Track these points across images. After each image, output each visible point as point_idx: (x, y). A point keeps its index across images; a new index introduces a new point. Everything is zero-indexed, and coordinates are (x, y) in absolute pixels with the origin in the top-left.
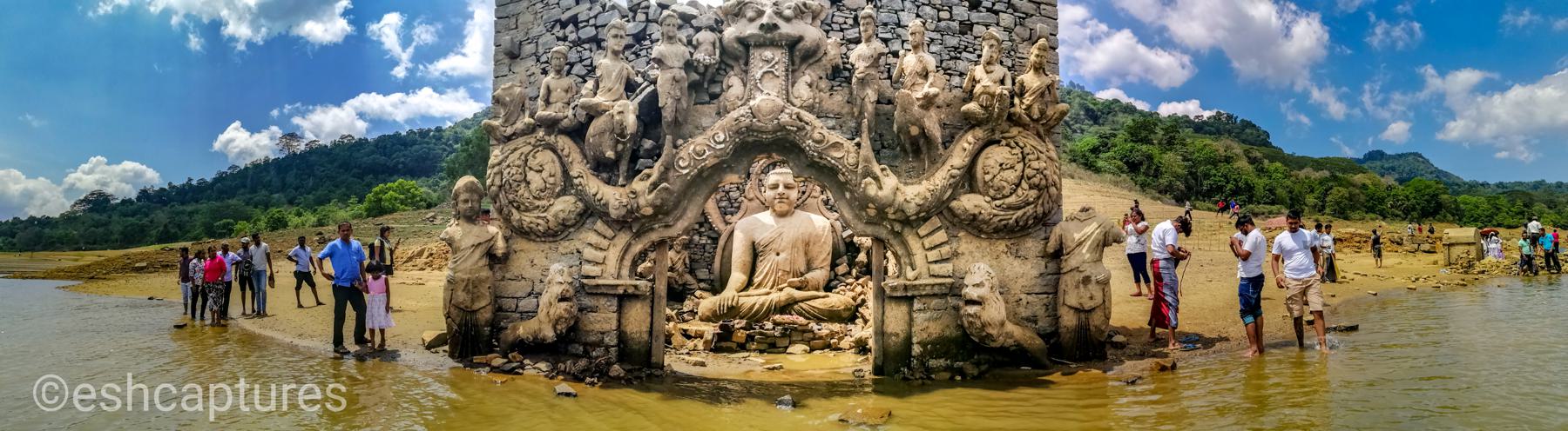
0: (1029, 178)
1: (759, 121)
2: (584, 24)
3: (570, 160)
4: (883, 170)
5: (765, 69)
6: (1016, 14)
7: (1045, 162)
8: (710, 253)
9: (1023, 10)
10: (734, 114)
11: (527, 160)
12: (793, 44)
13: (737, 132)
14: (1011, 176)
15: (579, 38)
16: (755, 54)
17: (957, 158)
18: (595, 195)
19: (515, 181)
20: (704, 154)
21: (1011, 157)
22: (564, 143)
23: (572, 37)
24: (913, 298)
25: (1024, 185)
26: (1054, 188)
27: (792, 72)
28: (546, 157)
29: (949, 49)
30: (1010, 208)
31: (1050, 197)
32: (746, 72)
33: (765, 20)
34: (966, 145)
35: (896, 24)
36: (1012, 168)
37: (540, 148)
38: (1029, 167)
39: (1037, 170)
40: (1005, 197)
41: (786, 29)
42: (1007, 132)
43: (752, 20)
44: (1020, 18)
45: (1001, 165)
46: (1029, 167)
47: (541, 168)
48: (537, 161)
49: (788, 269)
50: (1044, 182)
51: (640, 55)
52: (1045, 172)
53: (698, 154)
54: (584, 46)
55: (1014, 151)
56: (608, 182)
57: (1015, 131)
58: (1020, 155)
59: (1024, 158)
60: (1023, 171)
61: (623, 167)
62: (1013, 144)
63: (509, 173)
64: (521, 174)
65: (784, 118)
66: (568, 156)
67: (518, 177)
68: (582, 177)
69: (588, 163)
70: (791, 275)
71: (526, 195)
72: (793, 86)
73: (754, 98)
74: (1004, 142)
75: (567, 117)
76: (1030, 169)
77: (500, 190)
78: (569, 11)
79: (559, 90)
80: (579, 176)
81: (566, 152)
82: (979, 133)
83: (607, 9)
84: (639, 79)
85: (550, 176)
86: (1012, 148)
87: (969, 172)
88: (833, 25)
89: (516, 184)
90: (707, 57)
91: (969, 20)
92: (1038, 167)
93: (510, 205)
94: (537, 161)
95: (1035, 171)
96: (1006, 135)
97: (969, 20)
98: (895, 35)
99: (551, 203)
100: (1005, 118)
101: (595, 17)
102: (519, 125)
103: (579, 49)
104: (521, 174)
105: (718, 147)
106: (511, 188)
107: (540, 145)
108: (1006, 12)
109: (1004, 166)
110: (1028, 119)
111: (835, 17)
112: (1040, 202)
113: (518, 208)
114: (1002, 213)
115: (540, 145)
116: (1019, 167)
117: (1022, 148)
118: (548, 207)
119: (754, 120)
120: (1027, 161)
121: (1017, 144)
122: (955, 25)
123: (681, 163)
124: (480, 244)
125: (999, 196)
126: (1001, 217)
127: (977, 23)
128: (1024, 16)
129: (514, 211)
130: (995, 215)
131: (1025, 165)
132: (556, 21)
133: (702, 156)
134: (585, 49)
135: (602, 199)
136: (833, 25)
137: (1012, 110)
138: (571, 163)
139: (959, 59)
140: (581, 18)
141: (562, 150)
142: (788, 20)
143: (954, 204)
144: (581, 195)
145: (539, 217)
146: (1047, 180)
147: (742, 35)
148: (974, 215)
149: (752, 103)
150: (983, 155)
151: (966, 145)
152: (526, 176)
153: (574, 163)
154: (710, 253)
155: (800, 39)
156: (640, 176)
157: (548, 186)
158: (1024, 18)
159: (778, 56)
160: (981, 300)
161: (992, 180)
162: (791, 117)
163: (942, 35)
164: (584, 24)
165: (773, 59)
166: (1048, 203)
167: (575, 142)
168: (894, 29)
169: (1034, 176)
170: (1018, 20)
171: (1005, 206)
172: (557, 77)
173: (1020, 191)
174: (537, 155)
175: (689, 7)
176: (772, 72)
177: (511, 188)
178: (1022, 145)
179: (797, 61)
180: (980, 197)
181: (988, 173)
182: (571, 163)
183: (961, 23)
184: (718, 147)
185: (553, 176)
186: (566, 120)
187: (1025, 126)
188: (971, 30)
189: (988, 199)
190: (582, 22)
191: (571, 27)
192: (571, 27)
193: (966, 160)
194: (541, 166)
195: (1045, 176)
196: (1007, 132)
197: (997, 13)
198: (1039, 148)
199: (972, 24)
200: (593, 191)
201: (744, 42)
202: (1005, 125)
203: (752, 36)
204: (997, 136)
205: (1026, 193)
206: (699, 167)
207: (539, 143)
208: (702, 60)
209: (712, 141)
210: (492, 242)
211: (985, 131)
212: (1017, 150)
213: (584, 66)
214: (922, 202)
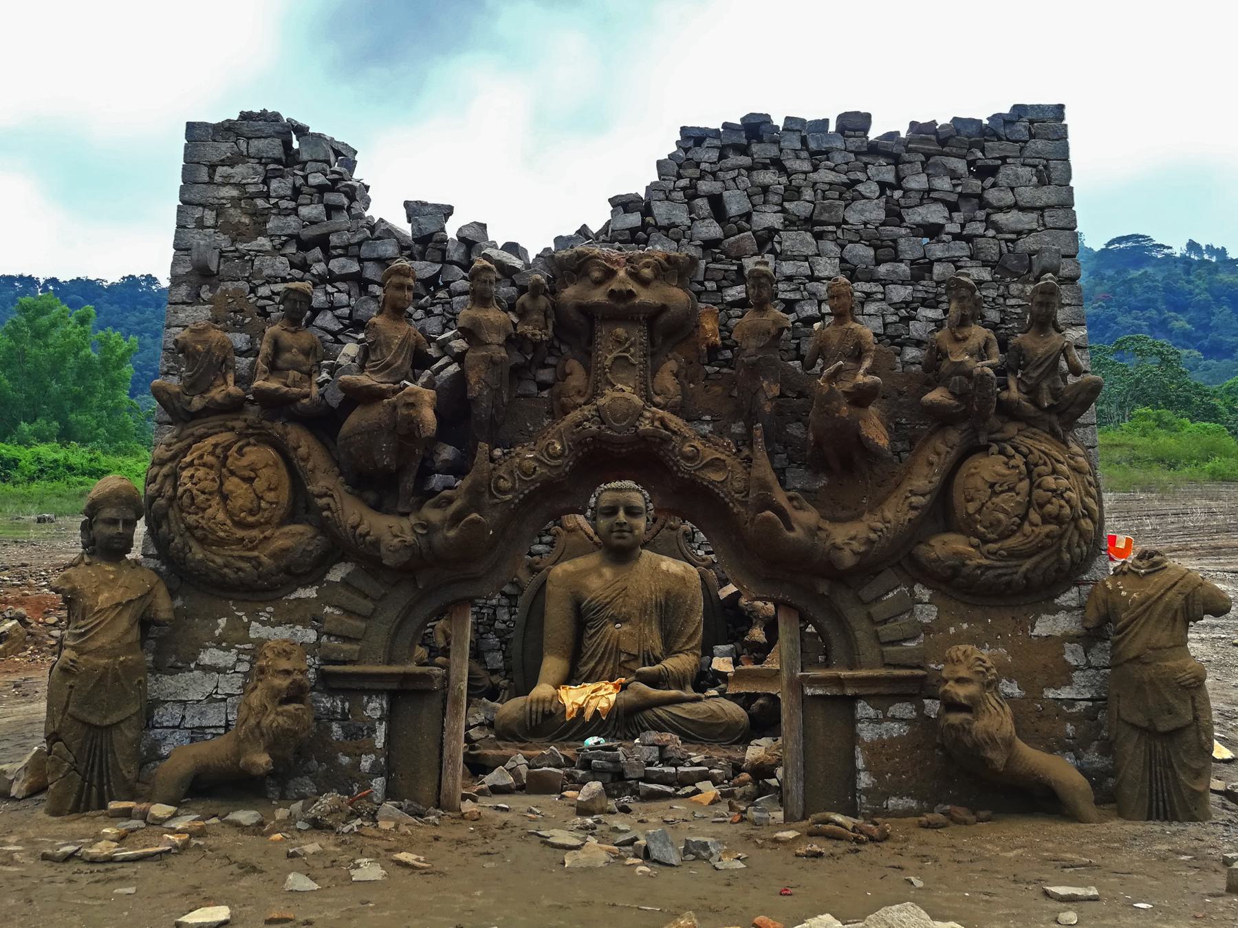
0: (1041, 506)
1: (609, 428)
2: (340, 251)
3: (310, 465)
4: (791, 499)
5: (615, 354)
6: (1000, 236)
7: (1068, 478)
8: (504, 622)
9: (1013, 226)
10: (575, 415)
11: (226, 458)
12: (653, 317)
13: (580, 443)
14: (1008, 501)
15: (330, 272)
16: (603, 331)
17: (923, 481)
18: (355, 528)
19: (203, 493)
20: (534, 473)
21: (1006, 472)
22: (303, 442)
23: (318, 268)
24: (855, 698)
25: (1034, 516)
26: (1088, 521)
27: (654, 356)
28: (258, 455)
29: (898, 306)
30: (1013, 554)
31: (1081, 535)
32: (589, 354)
33: (614, 286)
34: (933, 458)
35: (807, 277)
36: (1011, 489)
37: (252, 440)
38: (1039, 486)
39: (1053, 491)
40: (1003, 536)
41: (645, 296)
42: (998, 431)
43: (598, 283)
44: (1007, 241)
45: (992, 486)
46: (1039, 486)
47: (253, 474)
48: (245, 461)
49: (635, 652)
50: (1067, 510)
51: (431, 312)
52: (1068, 494)
53: (525, 474)
54: (337, 284)
55: (1012, 462)
56: (377, 507)
57: (1012, 429)
58: (1023, 468)
59: (1030, 472)
60: (1030, 494)
61: (408, 483)
62: (1010, 450)
63: (192, 477)
64: (213, 480)
65: (645, 426)
66: (306, 460)
67: (208, 485)
68: (332, 496)
69: (341, 474)
70: (641, 661)
71: (221, 516)
72: (654, 376)
73: (603, 395)
74: (995, 448)
75: (307, 396)
76: (1040, 491)
77: (170, 506)
78: (314, 227)
79: (294, 350)
80: (325, 495)
81: (303, 451)
82: (954, 436)
83: (377, 234)
84: (432, 351)
85: (270, 489)
86: (1008, 457)
87: (943, 498)
88: (706, 283)
89: (202, 497)
90: (537, 332)
91: (925, 257)
92: (1054, 487)
93: (188, 534)
94: (245, 461)
95: (1050, 493)
96: (998, 436)
97: (925, 257)
98: (805, 293)
99: (267, 533)
100: (993, 410)
101: (359, 244)
102: (217, 394)
103: (329, 289)
104: (213, 480)
105: (553, 463)
106: (193, 503)
107: (252, 435)
108: (984, 236)
109: (997, 488)
110: (1032, 408)
111: (709, 272)
112: (1065, 542)
113: (202, 541)
114: (998, 564)
115: (252, 435)
116: (1024, 485)
117: (1025, 456)
118: (261, 541)
119: (603, 427)
120: (1035, 474)
121: (1016, 449)
122: (904, 268)
123: (502, 483)
124: (131, 601)
125: (994, 536)
126: (1000, 571)
127: (939, 260)
128: (1013, 236)
129: (192, 543)
130: (988, 568)
131: (1032, 483)
132: (291, 237)
133: (530, 476)
134: (339, 291)
135: (368, 534)
136: (706, 283)
137: (1005, 395)
138: (312, 471)
139: (914, 319)
140: (334, 240)
141: (295, 449)
142: (645, 283)
143: (922, 550)
144: (324, 527)
145: (241, 558)
146: (1071, 507)
147: (584, 302)
148: (953, 568)
149: (601, 401)
150: (963, 471)
151: (933, 458)
152: (222, 484)
153: (316, 472)
154: (504, 622)
155: (663, 308)
156: (432, 500)
157: (263, 504)
158: (1013, 241)
159: (638, 335)
160: (970, 704)
161: (979, 511)
162: (652, 422)
163: (884, 286)
164: (340, 251)
165: (627, 339)
166: (1079, 546)
167: (320, 439)
168: (804, 284)
169: (1049, 502)
170: (1003, 244)
171: (1005, 553)
172: (293, 329)
173: (1027, 527)
174: (247, 449)
175: (505, 254)
176: (626, 358)
177: (193, 503)
178: (1025, 450)
179: (659, 340)
180: (961, 538)
181: (972, 500)
182: (312, 471)
183: (913, 262)
184: (553, 463)
185: (275, 489)
186: (305, 401)
187: (1030, 422)
188: (931, 272)
189: (975, 541)
190: (335, 248)
191: (317, 252)
192: (317, 252)
193: (936, 479)
194: (252, 470)
195: (1068, 502)
196: (1000, 430)
197: (969, 239)
198: (1054, 453)
199: (931, 263)
200: (352, 519)
201: (588, 312)
202: (994, 421)
203: (598, 305)
204: (983, 440)
205: (1037, 530)
206: (526, 492)
207: (251, 431)
208: (529, 335)
209: (545, 454)
210: (149, 600)
211: (963, 431)
212: (1018, 460)
213: (338, 317)
214: (862, 549)
